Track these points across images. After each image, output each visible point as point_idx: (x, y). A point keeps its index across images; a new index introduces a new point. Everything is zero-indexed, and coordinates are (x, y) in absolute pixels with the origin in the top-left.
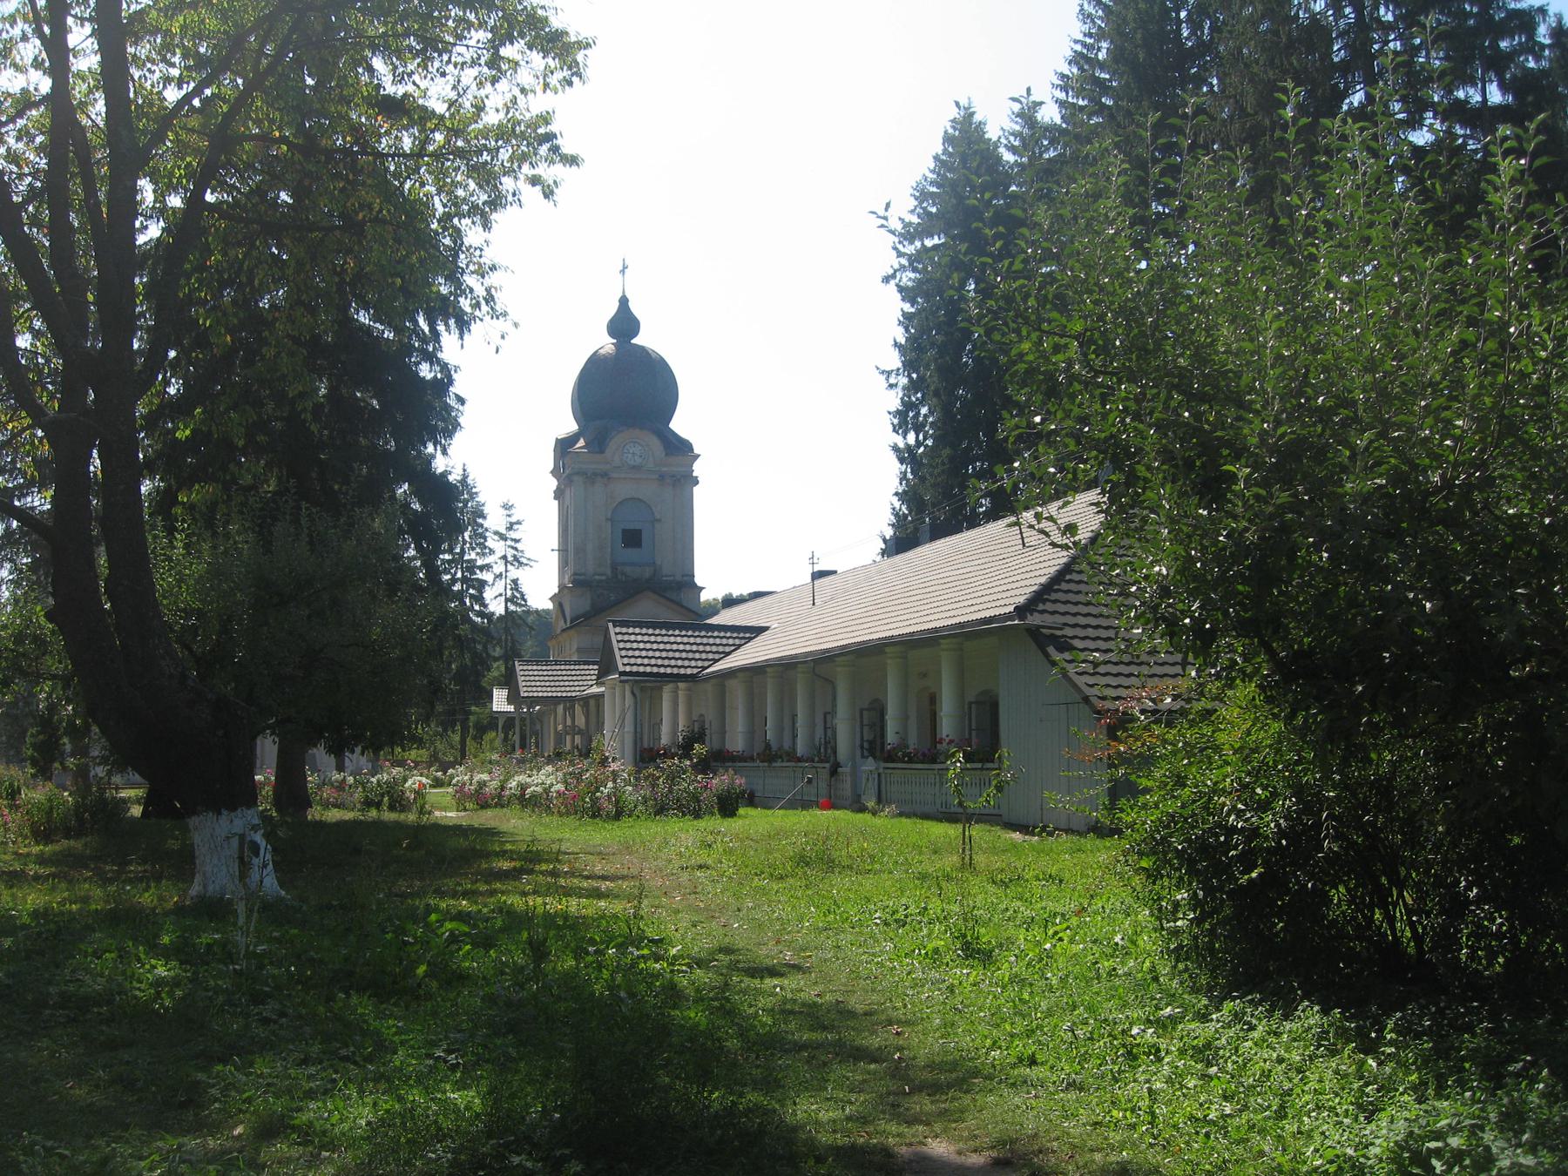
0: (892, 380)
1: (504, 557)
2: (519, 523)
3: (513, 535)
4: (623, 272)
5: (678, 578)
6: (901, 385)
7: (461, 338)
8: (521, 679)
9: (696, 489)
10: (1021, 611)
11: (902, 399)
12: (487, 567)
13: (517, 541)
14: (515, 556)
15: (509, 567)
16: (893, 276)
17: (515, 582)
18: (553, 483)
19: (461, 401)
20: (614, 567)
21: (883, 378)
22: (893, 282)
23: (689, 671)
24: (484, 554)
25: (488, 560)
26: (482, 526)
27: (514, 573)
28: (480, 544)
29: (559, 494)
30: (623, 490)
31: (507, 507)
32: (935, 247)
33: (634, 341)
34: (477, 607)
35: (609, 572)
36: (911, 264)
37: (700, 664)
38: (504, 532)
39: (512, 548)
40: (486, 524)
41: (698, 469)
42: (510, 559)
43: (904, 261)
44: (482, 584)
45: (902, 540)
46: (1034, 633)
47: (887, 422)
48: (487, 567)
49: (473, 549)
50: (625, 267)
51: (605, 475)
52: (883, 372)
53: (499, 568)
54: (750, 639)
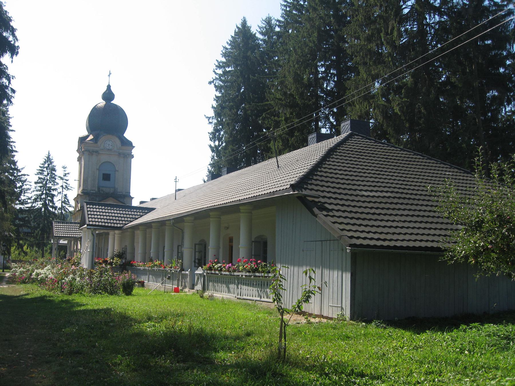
0: (210, 121)
1: (62, 186)
2: (68, 174)
3: (66, 178)
4: (109, 76)
5: (124, 193)
6: (214, 123)
7: (12, 57)
8: (54, 229)
9: (132, 160)
10: (293, 187)
11: (214, 128)
12: (55, 190)
13: (67, 180)
14: (66, 186)
15: (64, 190)
16: (213, 82)
17: (66, 195)
18: (77, 155)
19: (13, 91)
20: (99, 188)
21: (207, 120)
22: (212, 84)
23: (119, 225)
24: (54, 185)
25: (56, 187)
26: (54, 174)
27: (65, 192)
28: (53, 181)
29: (79, 159)
30: (104, 158)
31: (64, 168)
32: (229, 71)
33: (112, 102)
34: (51, 204)
35: (97, 190)
36: (220, 78)
37: (124, 222)
38: (62, 177)
39: (66, 183)
40: (56, 174)
41: (134, 152)
42: (64, 187)
43: (217, 77)
44: (53, 196)
45: (214, 175)
46: (302, 199)
47: (207, 137)
48: (55, 190)
49: (50, 182)
50: (110, 74)
51: (97, 152)
52: (207, 117)
53: (60, 190)
54: (147, 213)
